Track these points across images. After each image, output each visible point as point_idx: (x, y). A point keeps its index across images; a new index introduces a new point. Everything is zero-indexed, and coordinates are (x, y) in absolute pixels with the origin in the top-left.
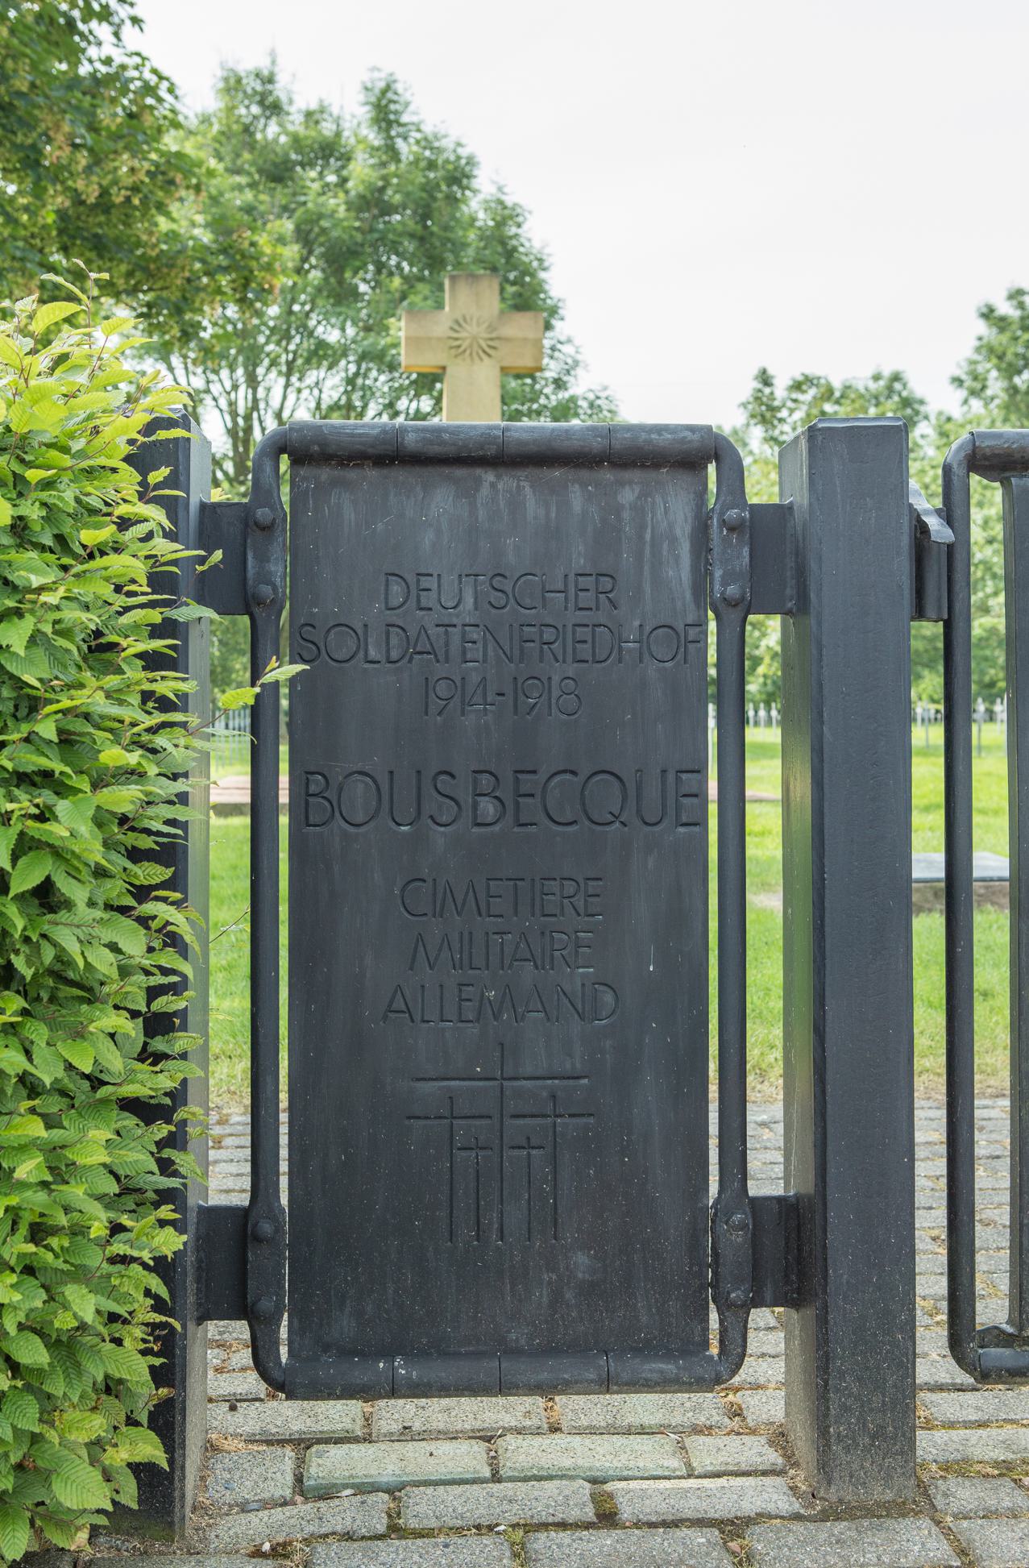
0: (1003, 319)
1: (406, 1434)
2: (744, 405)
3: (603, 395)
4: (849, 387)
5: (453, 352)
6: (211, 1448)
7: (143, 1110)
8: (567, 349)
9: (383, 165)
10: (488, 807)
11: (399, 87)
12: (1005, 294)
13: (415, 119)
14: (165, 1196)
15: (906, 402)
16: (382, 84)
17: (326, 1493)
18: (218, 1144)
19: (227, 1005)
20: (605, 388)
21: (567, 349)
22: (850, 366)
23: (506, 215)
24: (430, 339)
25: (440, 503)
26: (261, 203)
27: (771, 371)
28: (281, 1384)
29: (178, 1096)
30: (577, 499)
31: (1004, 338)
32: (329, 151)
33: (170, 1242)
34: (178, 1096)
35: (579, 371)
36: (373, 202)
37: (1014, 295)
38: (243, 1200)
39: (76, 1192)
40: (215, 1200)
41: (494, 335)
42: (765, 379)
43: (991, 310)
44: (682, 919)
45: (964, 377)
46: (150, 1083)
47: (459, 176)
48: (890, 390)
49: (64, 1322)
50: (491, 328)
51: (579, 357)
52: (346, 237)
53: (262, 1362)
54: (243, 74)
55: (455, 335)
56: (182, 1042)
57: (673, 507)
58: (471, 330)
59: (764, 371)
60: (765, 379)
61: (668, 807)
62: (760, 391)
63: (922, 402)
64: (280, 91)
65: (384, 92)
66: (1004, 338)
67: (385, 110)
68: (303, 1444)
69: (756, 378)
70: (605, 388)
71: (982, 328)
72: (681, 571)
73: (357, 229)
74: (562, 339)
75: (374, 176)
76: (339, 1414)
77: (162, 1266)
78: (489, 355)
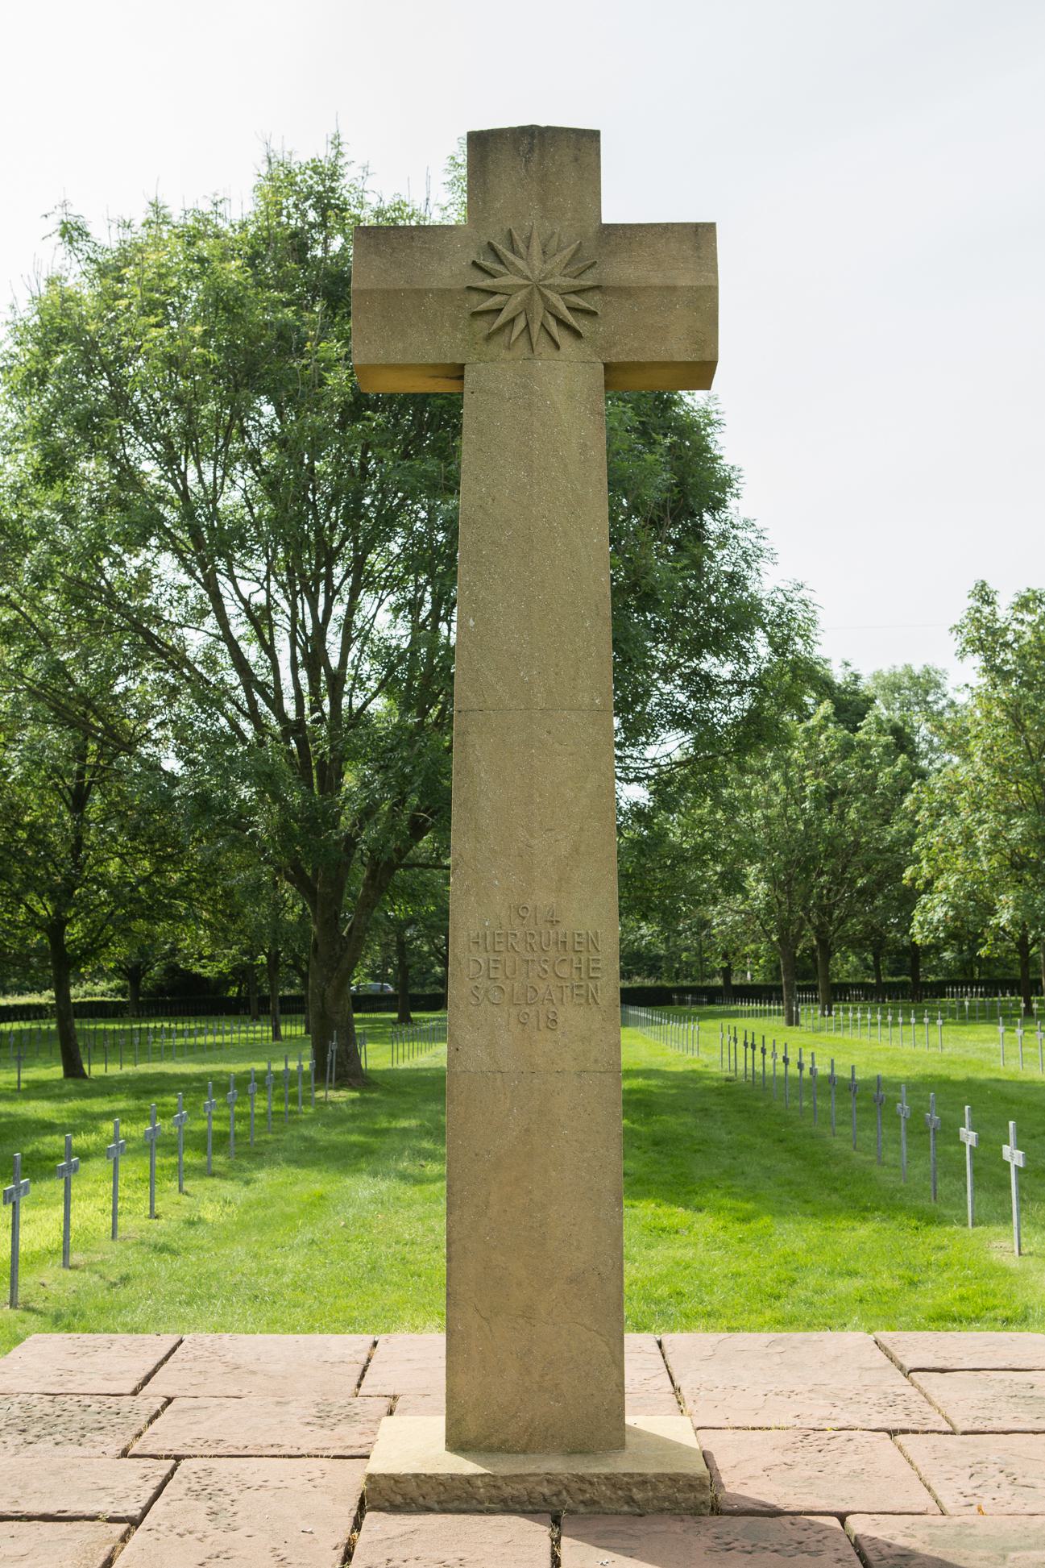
2: (958, 629)
3: (797, 596)
5: (483, 326)
20: (800, 587)
24: (421, 293)
27: (992, 585)
35: (762, 565)
37: (985, 638)
41: (587, 281)
42: (985, 595)
51: (762, 543)
54: (296, 168)
55: (487, 283)
60: (985, 595)
62: (978, 611)
64: (345, 188)
69: (972, 595)
70: (800, 587)
78: (577, 334)
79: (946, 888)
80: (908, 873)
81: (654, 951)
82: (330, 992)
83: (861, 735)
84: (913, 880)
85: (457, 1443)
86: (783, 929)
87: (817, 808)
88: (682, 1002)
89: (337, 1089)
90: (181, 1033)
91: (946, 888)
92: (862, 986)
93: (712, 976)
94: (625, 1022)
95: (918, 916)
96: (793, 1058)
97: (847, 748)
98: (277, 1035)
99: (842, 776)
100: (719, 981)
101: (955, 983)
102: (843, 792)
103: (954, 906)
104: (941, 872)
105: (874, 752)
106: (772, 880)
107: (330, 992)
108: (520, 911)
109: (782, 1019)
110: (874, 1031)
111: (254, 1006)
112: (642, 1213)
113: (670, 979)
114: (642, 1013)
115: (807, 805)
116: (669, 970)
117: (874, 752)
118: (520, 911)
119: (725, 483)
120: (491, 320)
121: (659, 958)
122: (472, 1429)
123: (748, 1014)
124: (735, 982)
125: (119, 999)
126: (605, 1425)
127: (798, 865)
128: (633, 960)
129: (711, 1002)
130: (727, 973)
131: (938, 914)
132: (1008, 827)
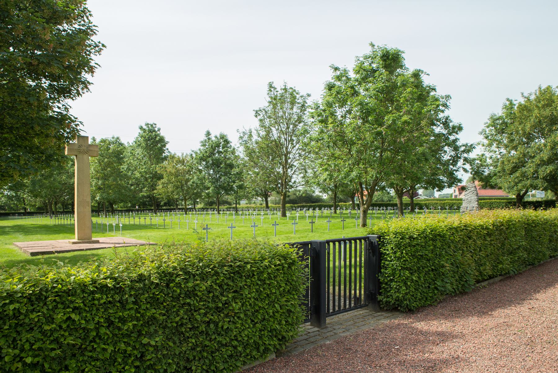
0: (144, 129)
27: (95, 138)
43: (142, 127)
48: (116, 141)
71: (139, 131)
94: (93, 216)
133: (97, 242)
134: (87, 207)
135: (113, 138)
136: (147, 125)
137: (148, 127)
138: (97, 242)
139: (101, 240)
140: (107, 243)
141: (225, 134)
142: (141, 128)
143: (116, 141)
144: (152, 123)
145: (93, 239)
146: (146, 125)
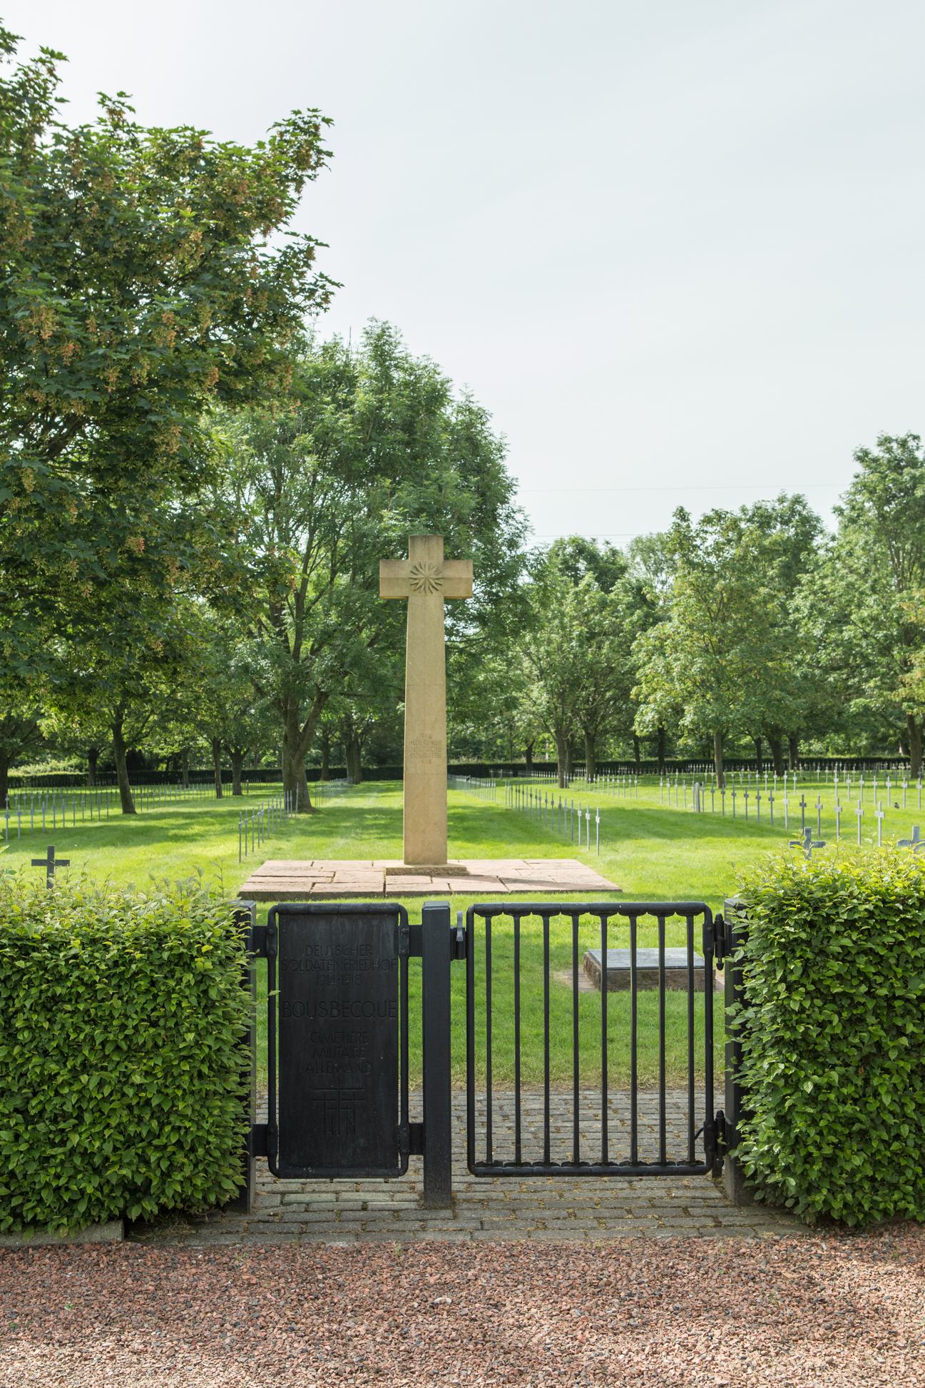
0: (875, 460)
1: (314, 1191)
4: (759, 508)
6: (257, 1194)
7: (241, 1098)
8: (519, 517)
9: (380, 391)
10: (335, 1012)
11: (392, 332)
12: (876, 441)
13: (403, 355)
14: (244, 1120)
15: (805, 520)
16: (378, 331)
17: (290, 1204)
18: (259, 1107)
19: (262, 1076)
21: (519, 517)
22: (765, 492)
23: (474, 417)
25: (322, 926)
26: (291, 419)
27: (687, 510)
28: (278, 1174)
29: (248, 1095)
30: (360, 923)
31: (875, 477)
32: (344, 377)
33: (248, 1130)
34: (248, 1095)
36: (373, 422)
38: (266, 1122)
39: (227, 1117)
40: (258, 1122)
42: (682, 515)
43: (866, 453)
44: (391, 1044)
45: (844, 507)
46: (242, 1091)
47: (436, 397)
48: (793, 511)
49: (224, 1147)
50: (438, 571)
52: (352, 447)
53: (272, 1168)
56: (249, 1079)
57: (388, 926)
58: (426, 572)
59: (682, 510)
60: (682, 515)
61: (389, 1008)
63: (818, 519)
65: (380, 337)
66: (875, 477)
67: (381, 349)
68: (283, 1194)
71: (859, 468)
72: (391, 945)
73: (359, 440)
74: (515, 509)
75: (372, 399)
76: (294, 1184)
77: (245, 1136)
79: (655, 701)
80: (634, 690)
81: (478, 737)
82: (294, 762)
83: (612, 596)
84: (637, 695)
85: (406, 863)
86: (558, 725)
87: (580, 646)
88: (496, 775)
89: (300, 812)
90: (145, 796)
91: (655, 701)
92: (628, 764)
93: (519, 756)
94: (451, 786)
95: (637, 718)
96: (550, 800)
97: (603, 604)
98: (219, 795)
99: (600, 624)
100: (524, 760)
101: (694, 762)
102: (599, 634)
103: (659, 713)
104: (655, 690)
105: (619, 608)
106: (551, 692)
107: (294, 762)
108: (422, 735)
109: (557, 784)
110: (616, 790)
111: (186, 778)
112: (449, 792)
113: (489, 758)
114: (461, 780)
115: (574, 643)
116: (487, 752)
117: (619, 608)
118: (422, 735)
119: (509, 487)
120: (416, 587)
121: (480, 742)
122: (410, 859)
123: (538, 783)
124: (535, 760)
125: (77, 773)
126: (444, 859)
127: (567, 682)
128: (458, 745)
129: (515, 775)
130: (529, 754)
131: (648, 718)
132: (692, 663)
133: (461, 873)
134: (434, 760)
135: (782, 500)
136: (885, 442)
137: (889, 450)
138: (461, 873)
139: (473, 866)
140: (515, 881)
141: (815, 514)
142: (863, 457)
143: (793, 511)
144: (902, 436)
145: (452, 862)
146: (880, 444)
